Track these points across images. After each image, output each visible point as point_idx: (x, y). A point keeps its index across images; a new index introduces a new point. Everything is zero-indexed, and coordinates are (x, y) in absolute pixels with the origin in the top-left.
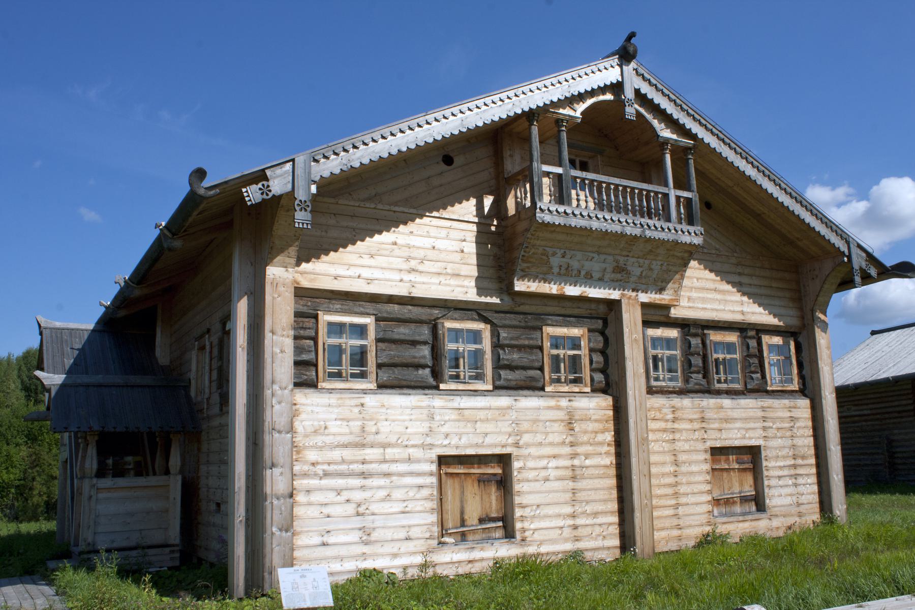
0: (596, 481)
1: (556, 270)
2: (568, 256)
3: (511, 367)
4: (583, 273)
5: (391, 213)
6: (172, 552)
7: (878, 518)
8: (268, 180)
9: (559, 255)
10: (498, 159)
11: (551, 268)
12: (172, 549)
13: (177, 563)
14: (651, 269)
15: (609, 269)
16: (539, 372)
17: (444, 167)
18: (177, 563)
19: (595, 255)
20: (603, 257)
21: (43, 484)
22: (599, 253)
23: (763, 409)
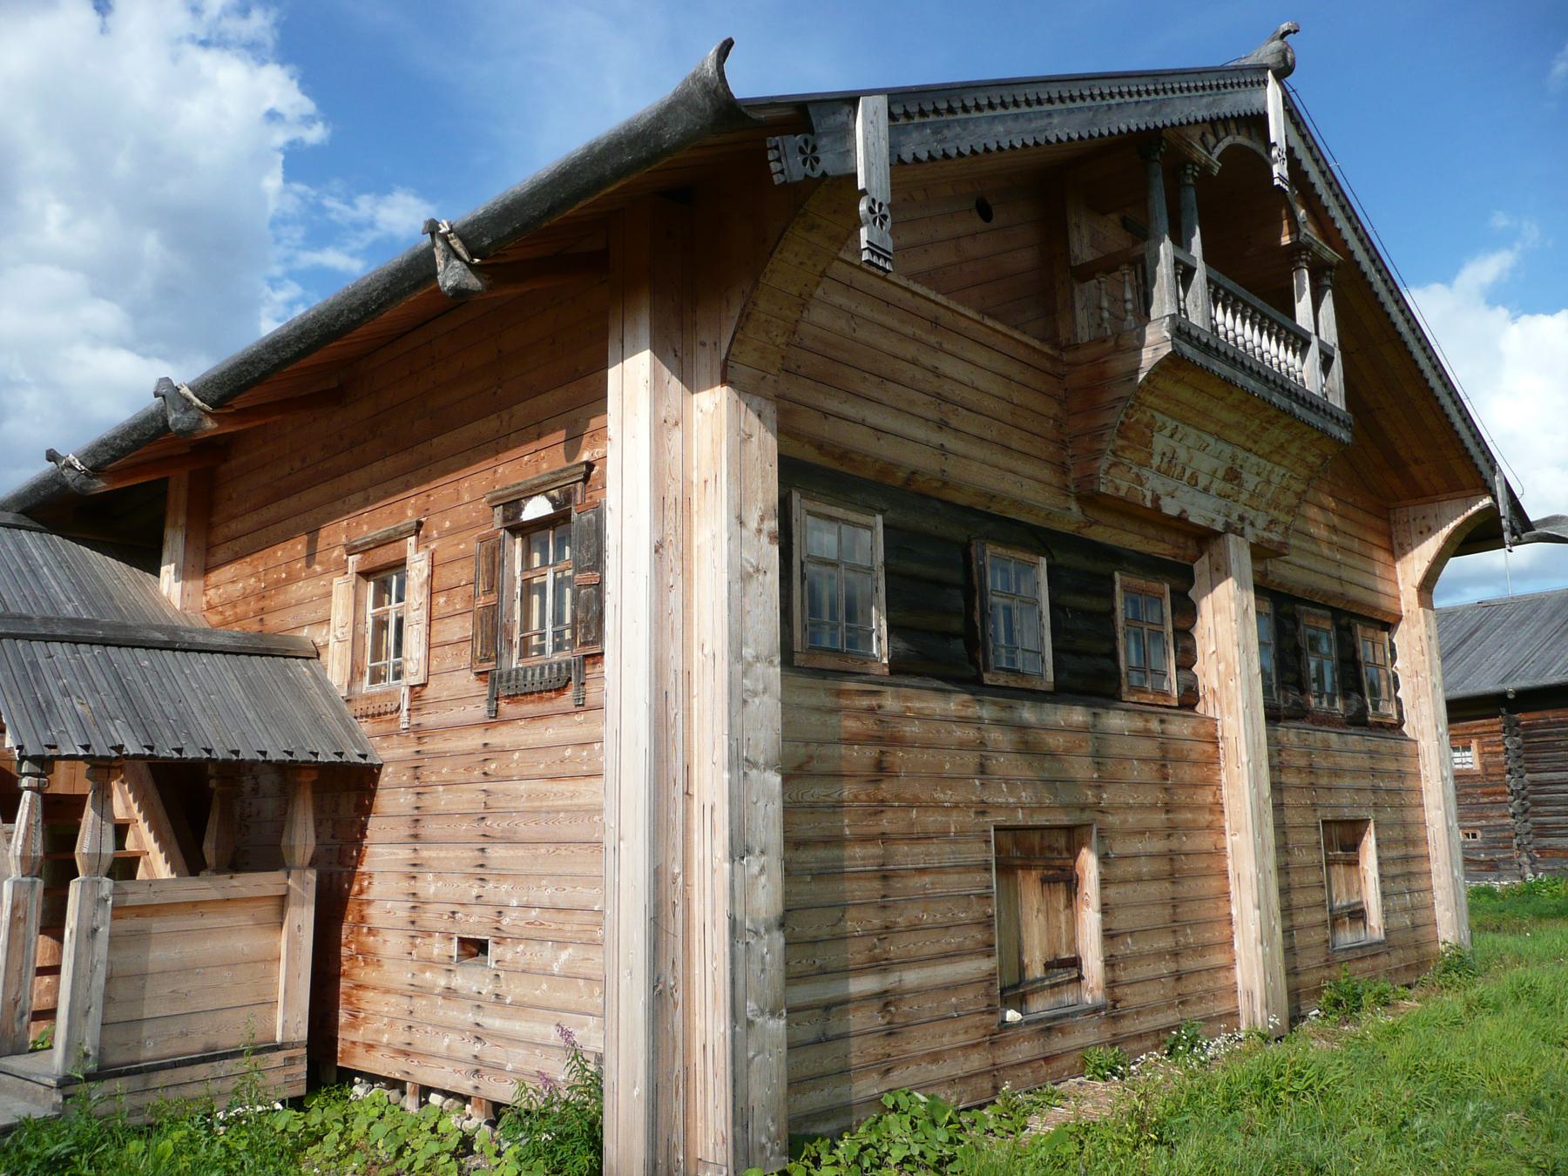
0: (953, 878)
1: (1156, 461)
2: (1178, 436)
3: (1077, 653)
4: (1188, 473)
5: (909, 295)
6: (291, 1060)
7: (1510, 940)
8: (811, 131)
9: (1167, 432)
10: (1053, 234)
11: (1151, 455)
12: (290, 1053)
13: (301, 1090)
14: (1269, 482)
15: (1221, 473)
16: (1109, 661)
17: (978, 223)
18: (301, 1090)
19: (1211, 441)
20: (1222, 446)
21: (1354, 988)
22: (1219, 437)
23: (1372, 753)
